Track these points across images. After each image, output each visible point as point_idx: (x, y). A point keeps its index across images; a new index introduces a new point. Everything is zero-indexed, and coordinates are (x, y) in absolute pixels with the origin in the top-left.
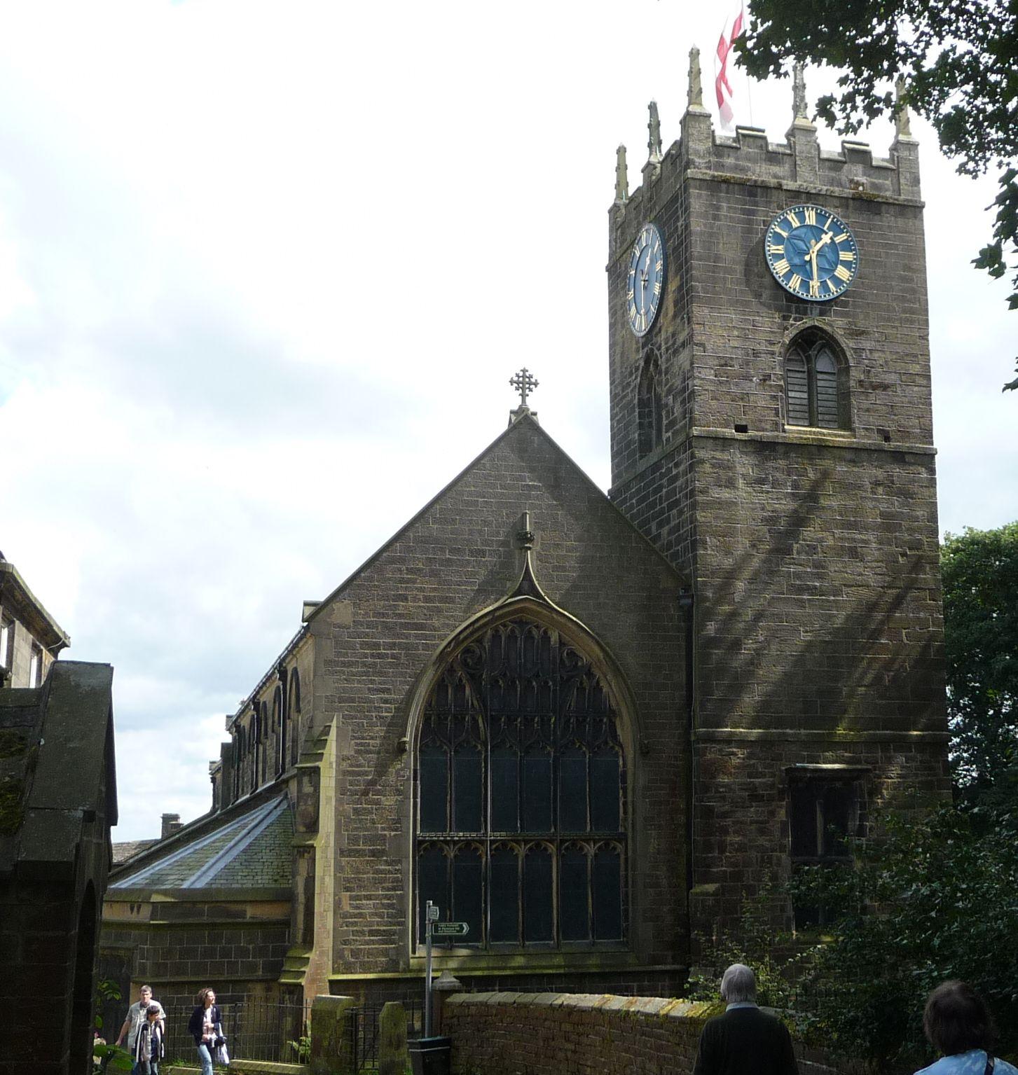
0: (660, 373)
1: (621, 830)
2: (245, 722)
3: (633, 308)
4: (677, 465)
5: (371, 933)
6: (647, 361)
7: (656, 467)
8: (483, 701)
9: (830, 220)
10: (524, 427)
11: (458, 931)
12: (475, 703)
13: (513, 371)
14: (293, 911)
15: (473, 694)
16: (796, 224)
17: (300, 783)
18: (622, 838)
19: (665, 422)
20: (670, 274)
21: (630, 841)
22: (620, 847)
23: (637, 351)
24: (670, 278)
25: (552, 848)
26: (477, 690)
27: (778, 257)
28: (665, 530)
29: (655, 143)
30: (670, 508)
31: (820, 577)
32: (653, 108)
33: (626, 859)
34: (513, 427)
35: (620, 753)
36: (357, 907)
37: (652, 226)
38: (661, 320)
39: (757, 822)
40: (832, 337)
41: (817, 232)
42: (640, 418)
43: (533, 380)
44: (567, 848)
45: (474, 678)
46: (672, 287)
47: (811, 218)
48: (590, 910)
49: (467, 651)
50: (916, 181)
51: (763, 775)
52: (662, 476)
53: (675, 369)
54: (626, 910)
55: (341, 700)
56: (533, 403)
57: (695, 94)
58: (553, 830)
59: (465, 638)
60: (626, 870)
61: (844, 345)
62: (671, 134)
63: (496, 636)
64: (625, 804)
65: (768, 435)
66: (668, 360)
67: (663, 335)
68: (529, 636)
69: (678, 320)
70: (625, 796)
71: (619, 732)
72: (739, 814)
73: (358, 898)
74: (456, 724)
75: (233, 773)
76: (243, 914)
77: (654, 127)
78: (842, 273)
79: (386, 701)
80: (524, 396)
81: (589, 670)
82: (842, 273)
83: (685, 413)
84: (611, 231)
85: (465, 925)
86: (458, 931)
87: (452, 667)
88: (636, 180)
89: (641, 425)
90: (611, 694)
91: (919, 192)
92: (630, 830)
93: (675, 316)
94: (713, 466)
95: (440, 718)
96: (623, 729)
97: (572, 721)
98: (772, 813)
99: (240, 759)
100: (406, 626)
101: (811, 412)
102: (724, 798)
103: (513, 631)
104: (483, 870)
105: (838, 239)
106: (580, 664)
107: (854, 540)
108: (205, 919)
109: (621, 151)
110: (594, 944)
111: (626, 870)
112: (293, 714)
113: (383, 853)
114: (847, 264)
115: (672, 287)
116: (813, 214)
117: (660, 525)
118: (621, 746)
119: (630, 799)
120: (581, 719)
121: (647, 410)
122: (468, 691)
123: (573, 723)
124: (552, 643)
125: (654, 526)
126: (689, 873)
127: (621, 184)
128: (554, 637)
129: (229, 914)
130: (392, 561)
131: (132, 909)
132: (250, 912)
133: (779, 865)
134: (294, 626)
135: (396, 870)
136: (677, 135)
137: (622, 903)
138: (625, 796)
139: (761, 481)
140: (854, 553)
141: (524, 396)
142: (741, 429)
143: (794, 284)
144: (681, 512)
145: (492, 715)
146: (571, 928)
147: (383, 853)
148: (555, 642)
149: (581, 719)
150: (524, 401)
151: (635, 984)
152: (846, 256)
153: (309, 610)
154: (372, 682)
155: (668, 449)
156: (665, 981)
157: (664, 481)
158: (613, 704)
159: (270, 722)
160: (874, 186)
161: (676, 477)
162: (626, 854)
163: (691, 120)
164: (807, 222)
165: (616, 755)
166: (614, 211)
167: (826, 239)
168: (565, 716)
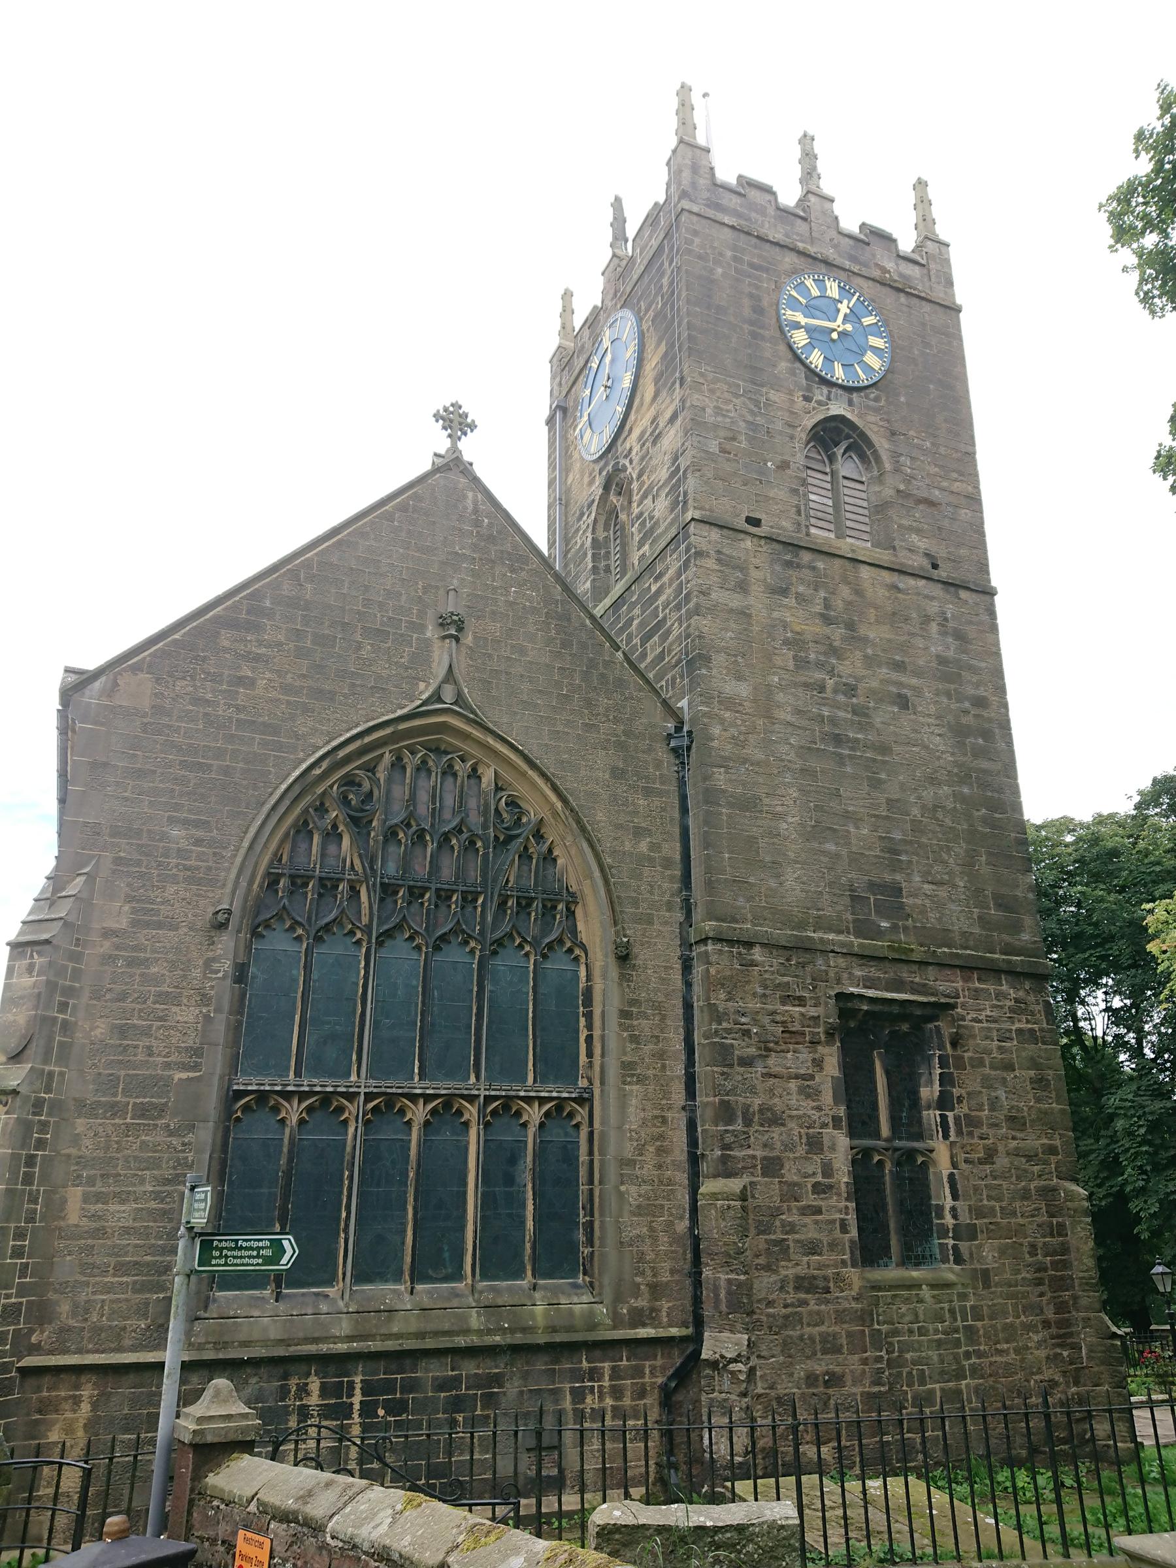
5: (120, 1269)
9: (855, 298)
10: (452, 466)
11: (268, 1261)
12: (357, 862)
15: (355, 850)
16: (815, 292)
18: (584, 1100)
21: (597, 1103)
22: (582, 1113)
25: (471, 1112)
31: (862, 727)
33: (591, 1134)
34: (436, 470)
35: (583, 960)
36: (94, 1217)
39: (797, 1077)
40: (863, 435)
42: (593, 561)
43: (469, 420)
44: (494, 1113)
45: (359, 823)
48: (530, 1224)
50: (950, 283)
51: (801, 1001)
56: (469, 448)
58: (473, 1079)
59: (348, 759)
60: (591, 1153)
61: (877, 445)
64: (589, 1039)
70: (590, 1027)
71: (580, 926)
72: (771, 1061)
73: (100, 1198)
74: (320, 895)
79: (198, 842)
81: (538, 831)
85: (289, 1245)
86: (268, 1261)
87: (322, 804)
90: (570, 869)
91: (953, 295)
92: (597, 1083)
95: (293, 884)
96: (586, 922)
97: (510, 904)
98: (818, 1063)
102: (747, 1033)
104: (348, 1149)
106: (524, 820)
107: (900, 684)
110: (534, 1287)
111: (591, 1153)
113: (162, 1110)
115: (652, 363)
116: (835, 285)
119: (597, 1033)
120: (524, 903)
121: (603, 552)
122: (346, 842)
123: (511, 908)
124: (483, 786)
126: (694, 1160)
128: (488, 776)
133: (833, 1148)
135: (184, 1144)
137: (582, 1213)
138: (590, 1027)
139: (784, 592)
140: (903, 703)
141: (454, 449)
143: (816, 359)
145: (381, 884)
146: (498, 1259)
147: (162, 1110)
148: (489, 785)
149: (524, 903)
151: (606, 1365)
153: (72, 678)
156: (655, 1359)
162: (591, 1124)
164: (829, 293)
165: (576, 959)
168: (500, 895)
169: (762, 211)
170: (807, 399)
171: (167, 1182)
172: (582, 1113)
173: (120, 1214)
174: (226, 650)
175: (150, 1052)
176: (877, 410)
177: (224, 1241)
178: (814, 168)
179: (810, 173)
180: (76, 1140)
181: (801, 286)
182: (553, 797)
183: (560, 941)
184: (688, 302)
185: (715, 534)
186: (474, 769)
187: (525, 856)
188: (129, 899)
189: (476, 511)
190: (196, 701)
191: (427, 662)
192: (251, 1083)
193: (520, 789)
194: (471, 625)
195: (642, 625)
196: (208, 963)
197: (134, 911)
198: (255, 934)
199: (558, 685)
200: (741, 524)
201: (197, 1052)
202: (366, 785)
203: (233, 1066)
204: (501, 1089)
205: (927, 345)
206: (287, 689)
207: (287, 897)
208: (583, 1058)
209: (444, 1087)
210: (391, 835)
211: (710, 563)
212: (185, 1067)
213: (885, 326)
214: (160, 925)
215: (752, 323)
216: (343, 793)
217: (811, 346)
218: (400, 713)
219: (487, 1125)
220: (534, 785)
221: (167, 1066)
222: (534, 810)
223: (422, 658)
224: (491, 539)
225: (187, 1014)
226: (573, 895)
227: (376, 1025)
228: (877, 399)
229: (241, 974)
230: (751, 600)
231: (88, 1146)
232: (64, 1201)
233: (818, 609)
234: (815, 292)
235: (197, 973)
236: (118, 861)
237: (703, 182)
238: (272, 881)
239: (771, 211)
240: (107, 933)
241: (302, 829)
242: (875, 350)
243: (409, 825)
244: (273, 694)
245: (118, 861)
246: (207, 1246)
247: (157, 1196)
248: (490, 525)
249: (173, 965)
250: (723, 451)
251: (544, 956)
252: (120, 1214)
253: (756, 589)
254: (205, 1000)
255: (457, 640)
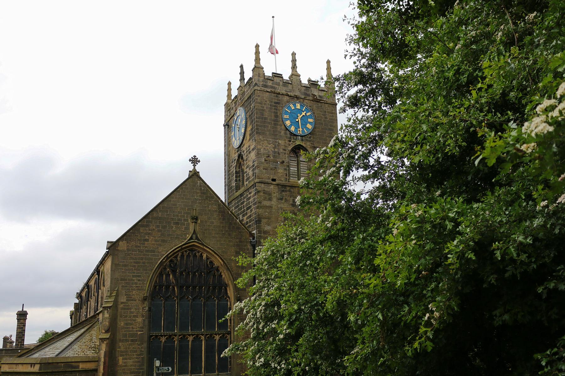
0: (244, 161)
1: (229, 330)
2: (84, 294)
3: (234, 138)
4: (250, 193)
6: (239, 157)
7: (241, 195)
8: (176, 280)
10: (194, 175)
13: (191, 156)
14: (99, 366)
16: (293, 108)
17: (103, 315)
19: (245, 178)
20: (249, 124)
22: (228, 337)
23: (235, 153)
24: (248, 126)
25: (203, 338)
26: (174, 276)
27: (287, 119)
28: (245, 218)
29: (242, 79)
30: (248, 209)
32: (242, 67)
34: (190, 177)
36: (125, 363)
37: (241, 108)
38: (244, 141)
41: (300, 111)
45: (174, 272)
46: (249, 129)
47: (298, 106)
48: (217, 361)
49: (171, 261)
52: (244, 198)
53: (249, 159)
54: (231, 361)
55: (122, 280)
56: (198, 168)
57: (257, 60)
62: (248, 75)
63: (182, 256)
65: (284, 182)
66: (247, 156)
67: (245, 147)
68: (195, 256)
69: (251, 141)
71: (228, 292)
73: (126, 359)
75: (78, 314)
76: (78, 367)
77: (242, 73)
78: (309, 126)
79: (139, 280)
80: (194, 166)
82: (309, 126)
83: (254, 174)
84: (225, 112)
88: (235, 93)
89: (236, 180)
93: (250, 140)
94: (264, 193)
99: (81, 308)
100: (147, 251)
101: (298, 175)
103: (189, 254)
105: (308, 114)
108: (61, 369)
109: (229, 84)
112: (102, 287)
113: (136, 340)
114: (310, 123)
115: (249, 129)
116: (299, 105)
117: (243, 216)
118: (229, 297)
122: (171, 276)
125: (241, 216)
127: (229, 95)
128: (204, 256)
129: (75, 367)
130: (143, 226)
131: (31, 366)
132: (82, 366)
134: (103, 251)
136: (250, 75)
139: (282, 199)
141: (194, 166)
142: (274, 180)
143: (293, 129)
144: (251, 211)
147: (136, 340)
150: (194, 168)
152: (310, 120)
153: (110, 245)
154: (134, 273)
155: (246, 188)
157: (245, 200)
158: (226, 281)
159: (93, 292)
160: (320, 96)
161: (250, 198)
163: (258, 68)
165: (227, 300)
166: (227, 105)
167: (304, 114)
169: (278, 84)
170: (290, 141)
171: (139, 355)
172: (228, 337)
173: (130, 362)
174: (142, 233)
175: (133, 328)
176: (310, 141)
177: (161, 368)
178: (295, 65)
179: (294, 67)
180: (120, 347)
181: (289, 108)
182: (221, 261)
183: (223, 296)
184: (257, 118)
185: (263, 185)
186: (201, 254)
187: (214, 276)
188: (126, 295)
189: (200, 186)
190: (136, 246)
191: (189, 229)
192: (154, 333)
193: (213, 259)
194: (200, 217)
195: (247, 205)
196: (143, 308)
197: (127, 297)
198: (152, 300)
199: (222, 231)
200: (270, 181)
201: (142, 328)
202: (175, 261)
203: (149, 330)
204: (209, 332)
205: (326, 118)
206: (156, 241)
207: (158, 291)
208: (229, 324)
209: (196, 332)
210: (181, 273)
211: (261, 194)
212: (140, 331)
213: (314, 115)
214: (132, 300)
215: (274, 121)
216: (171, 264)
217: (291, 125)
218: (183, 243)
219: (206, 340)
220: (216, 258)
221: (136, 331)
222: (216, 264)
223: (187, 228)
224: (204, 193)
225: (140, 320)
226: (226, 284)
227: (180, 319)
228: (310, 138)
229: (150, 309)
230: (273, 203)
231: (122, 349)
232: (119, 360)
233: (291, 202)
234: (293, 108)
235: (141, 310)
236: (123, 286)
237: (262, 79)
238: (155, 287)
239: (281, 83)
240: (122, 303)
241: (161, 275)
242: (310, 123)
243: (185, 270)
244: (153, 242)
245: (123, 286)
246: (158, 369)
247: (137, 358)
248: (204, 189)
249: (136, 309)
250: (265, 160)
251: (219, 300)
252: (130, 362)
253: (274, 199)
254: (143, 316)
255: (196, 222)
